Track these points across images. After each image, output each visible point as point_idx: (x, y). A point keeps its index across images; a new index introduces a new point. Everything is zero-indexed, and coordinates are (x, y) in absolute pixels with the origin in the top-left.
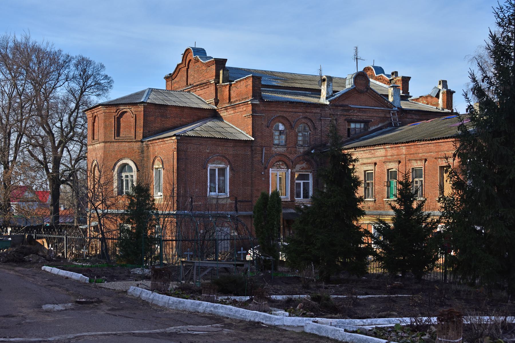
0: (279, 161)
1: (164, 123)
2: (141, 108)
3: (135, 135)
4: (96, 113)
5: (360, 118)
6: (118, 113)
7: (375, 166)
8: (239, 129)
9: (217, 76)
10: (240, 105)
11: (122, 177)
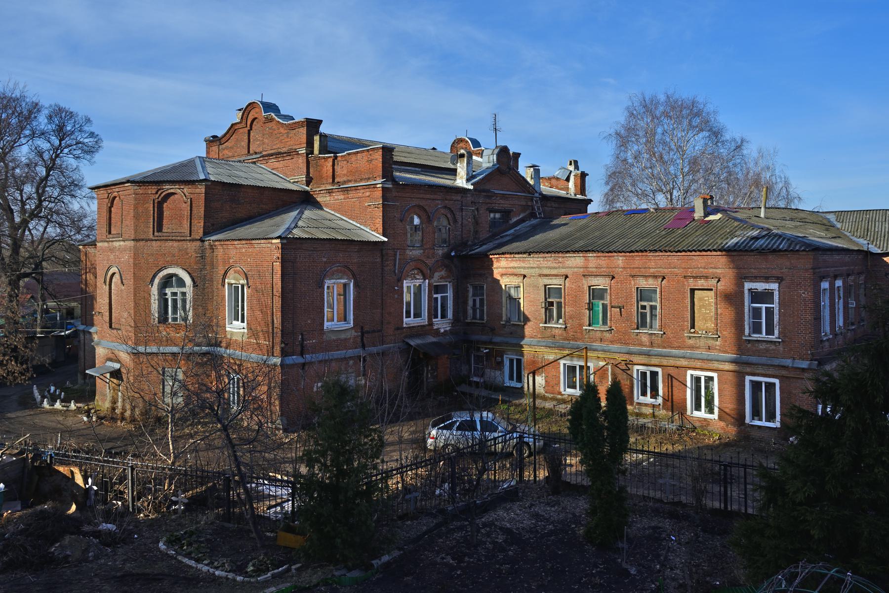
0: (413, 269)
1: (235, 210)
2: (201, 189)
3: (190, 231)
4: (116, 193)
5: (502, 207)
6: (160, 195)
7: (565, 280)
8: (355, 223)
9: (310, 144)
10: (359, 188)
11: (166, 294)
